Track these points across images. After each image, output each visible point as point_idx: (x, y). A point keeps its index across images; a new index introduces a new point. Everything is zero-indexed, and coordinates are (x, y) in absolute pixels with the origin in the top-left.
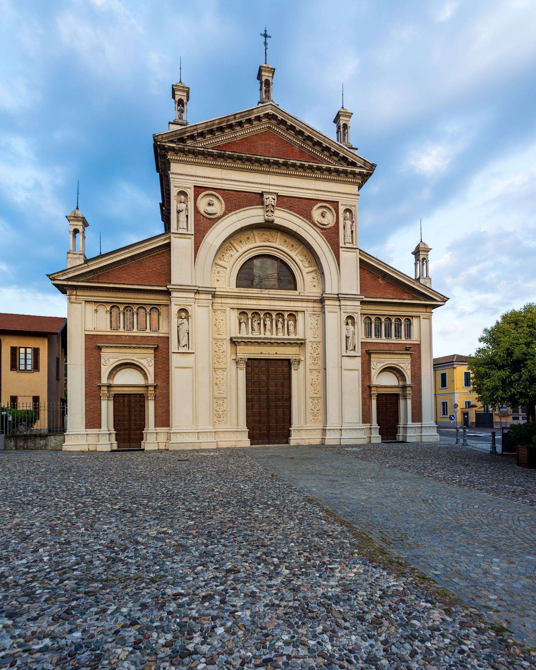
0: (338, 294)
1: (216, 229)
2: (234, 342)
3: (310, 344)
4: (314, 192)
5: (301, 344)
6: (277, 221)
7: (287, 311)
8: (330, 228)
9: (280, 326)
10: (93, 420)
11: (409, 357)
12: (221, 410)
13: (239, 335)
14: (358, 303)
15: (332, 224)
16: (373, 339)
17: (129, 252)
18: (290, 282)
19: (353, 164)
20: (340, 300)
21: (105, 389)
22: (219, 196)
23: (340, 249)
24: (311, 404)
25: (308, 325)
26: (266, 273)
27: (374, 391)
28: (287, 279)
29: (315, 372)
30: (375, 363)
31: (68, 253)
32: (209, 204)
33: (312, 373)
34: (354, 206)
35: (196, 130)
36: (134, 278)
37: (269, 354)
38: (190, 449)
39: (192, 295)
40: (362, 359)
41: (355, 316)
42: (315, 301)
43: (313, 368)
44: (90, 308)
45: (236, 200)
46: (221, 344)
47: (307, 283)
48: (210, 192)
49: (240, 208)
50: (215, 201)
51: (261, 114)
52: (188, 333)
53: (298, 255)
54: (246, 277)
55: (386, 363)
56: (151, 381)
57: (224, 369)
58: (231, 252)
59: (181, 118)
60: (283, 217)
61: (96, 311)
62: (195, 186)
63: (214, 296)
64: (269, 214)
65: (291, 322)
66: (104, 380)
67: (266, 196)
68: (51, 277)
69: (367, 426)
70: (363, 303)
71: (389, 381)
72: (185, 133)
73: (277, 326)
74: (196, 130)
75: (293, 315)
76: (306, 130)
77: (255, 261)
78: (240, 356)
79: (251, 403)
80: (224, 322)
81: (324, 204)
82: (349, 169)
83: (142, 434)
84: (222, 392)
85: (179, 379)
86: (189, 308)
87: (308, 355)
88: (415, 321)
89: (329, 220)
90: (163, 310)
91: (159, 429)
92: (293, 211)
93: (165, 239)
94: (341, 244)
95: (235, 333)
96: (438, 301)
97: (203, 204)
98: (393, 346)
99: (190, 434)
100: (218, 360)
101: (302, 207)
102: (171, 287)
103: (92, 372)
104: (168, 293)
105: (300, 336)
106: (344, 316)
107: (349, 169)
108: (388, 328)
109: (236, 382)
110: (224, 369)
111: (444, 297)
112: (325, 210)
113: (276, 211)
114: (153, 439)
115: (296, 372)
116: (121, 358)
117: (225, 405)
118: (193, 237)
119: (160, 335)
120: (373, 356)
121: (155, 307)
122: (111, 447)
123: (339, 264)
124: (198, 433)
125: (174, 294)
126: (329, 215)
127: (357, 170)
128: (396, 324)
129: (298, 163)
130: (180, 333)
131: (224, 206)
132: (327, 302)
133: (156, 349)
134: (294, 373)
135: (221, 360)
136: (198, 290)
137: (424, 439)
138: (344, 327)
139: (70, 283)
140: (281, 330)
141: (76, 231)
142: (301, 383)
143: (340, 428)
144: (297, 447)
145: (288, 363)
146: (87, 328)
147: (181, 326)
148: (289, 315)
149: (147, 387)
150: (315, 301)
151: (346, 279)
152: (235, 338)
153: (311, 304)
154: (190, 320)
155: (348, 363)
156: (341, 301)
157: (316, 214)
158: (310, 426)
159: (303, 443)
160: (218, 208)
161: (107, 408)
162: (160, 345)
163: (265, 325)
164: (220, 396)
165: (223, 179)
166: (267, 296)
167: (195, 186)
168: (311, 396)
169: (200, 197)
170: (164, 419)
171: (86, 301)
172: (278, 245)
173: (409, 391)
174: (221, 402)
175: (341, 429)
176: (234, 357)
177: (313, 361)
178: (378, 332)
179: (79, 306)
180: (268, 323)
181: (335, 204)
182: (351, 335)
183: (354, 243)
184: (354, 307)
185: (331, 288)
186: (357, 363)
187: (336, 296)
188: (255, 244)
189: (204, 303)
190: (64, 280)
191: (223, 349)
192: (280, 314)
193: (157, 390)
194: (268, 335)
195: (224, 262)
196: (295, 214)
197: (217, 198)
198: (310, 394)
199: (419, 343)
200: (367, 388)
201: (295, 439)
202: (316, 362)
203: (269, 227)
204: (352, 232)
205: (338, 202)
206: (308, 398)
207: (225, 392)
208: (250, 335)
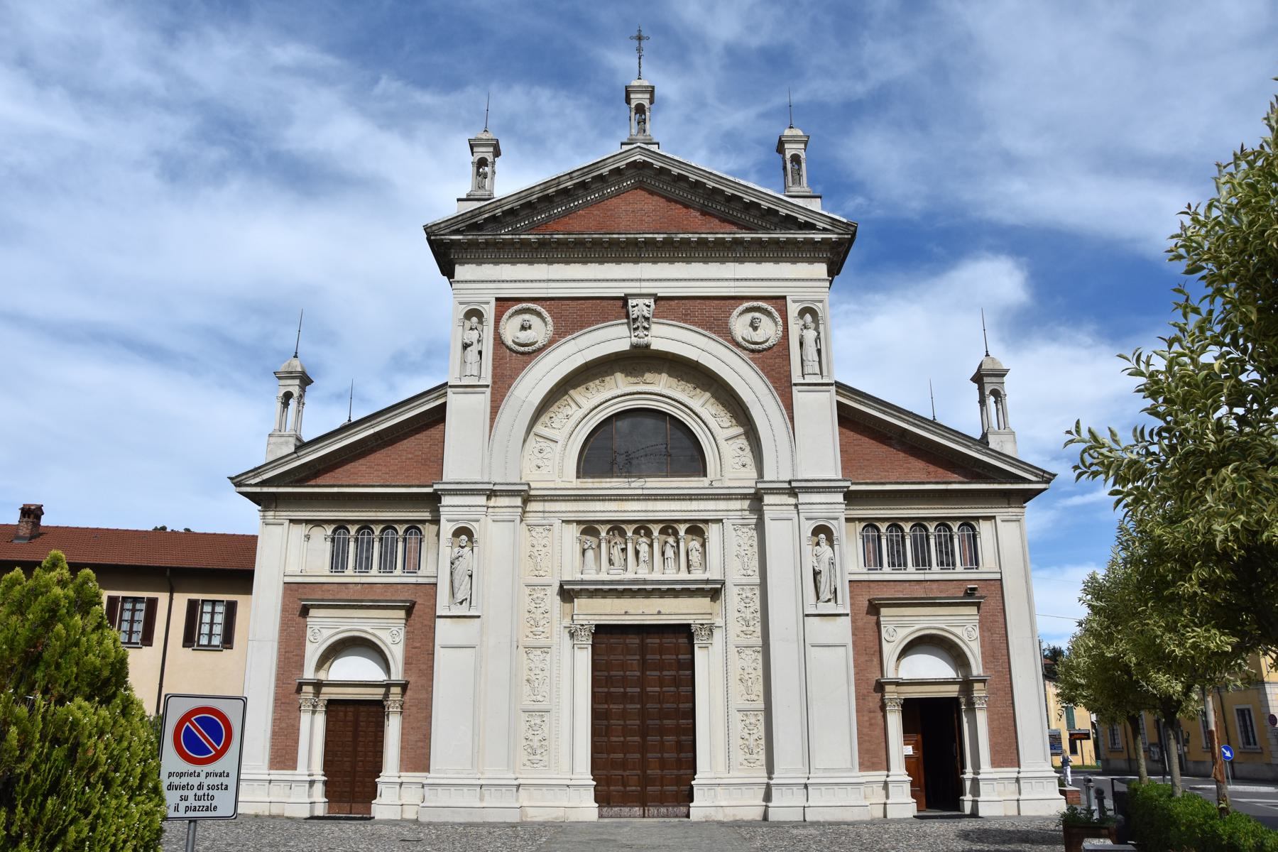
0: (790, 482)
1: (538, 367)
2: (567, 594)
3: (736, 590)
4: (732, 284)
5: (714, 592)
6: (657, 345)
7: (685, 521)
8: (770, 348)
9: (670, 552)
10: (283, 755)
11: (974, 610)
12: (537, 738)
13: (578, 577)
14: (839, 498)
16: (887, 573)
17: (372, 427)
19: (809, 226)
21: (310, 689)
22: (545, 314)
23: (794, 388)
24: (741, 725)
25: (732, 548)
26: (638, 445)
27: (891, 692)
28: (685, 453)
29: (749, 651)
30: (891, 628)
31: (270, 435)
32: (523, 328)
33: (743, 655)
34: (821, 301)
35: (500, 206)
36: (372, 478)
37: (643, 614)
38: (462, 820)
39: (482, 500)
40: (853, 622)
41: (832, 525)
42: (744, 497)
43: (745, 644)
44: (301, 530)
45: (573, 314)
46: (541, 595)
47: (727, 459)
48: (524, 305)
49: (582, 328)
50: (534, 320)
52: (471, 576)
53: (708, 405)
54: (604, 452)
55: (917, 627)
56: (397, 674)
57: (545, 649)
58: (568, 411)
59: (481, 187)
60: (667, 337)
61: (308, 537)
62: (498, 299)
63: (527, 499)
64: (641, 333)
66: (309, 673)
67: (631, 302)
68: (237, 481)
69: (880, 776)
70: (852, 498)
72: (480, 214)
73: (663, 554)
74: (500, 206)
75: (696, 529)
76: (709, 179)
77: (619, 424)
78: (580, 620)
79: (605, 722)
80: (549, 549)
81: (755, 304)
82: (800, 236)
83: (375, 786)
84: (539, 698)
85: (449, 668)
86: (474, 527)
87: (732, 615)
88: (984, 529)
89: (768, 331)
90: (428, 530)
91: (408, 777)
92: (691, 323)
93: (437, 398)
94: (796, 378)
95: (572, 571)
96: (1030, 482)
97: (511, 331)
98: (935, 585)
99: (465, 789)
100: (534, 629)
101: (709, 313)
102: (441, 487)
103: (290, 655)
104: (433, 500)
105: (714, 574)
106: (808, 527)
107: (800, 236)
108: (922, 546)
109: (573, 674)
110: (545, 649)
111: (1044, 472)
112: (757, 315)
113: (654, 327)
114: (395, 796)
115: (705, 651)
116: (343, 628)
117: (546, 727)
118: (489, 390)
119: (421, 580)
120: (884, 611)
121: (413, 526)
122: (312, 810)
123: (792, 419)
124: (481, 786)
125: (446, 500)
127: (818, 237)
128: (915, 537)
130: (456, 577)
131: (550, 327)
132: (768, 499)
133: (409, 610)
134: (699, 655)
135: (541, 629)
136: (492, 490)
137: (1027, 810)
138: (808, 549)
139: (265, 490)
140: (671, 563)
141: (288, 396)
142: (717, 680)
143: (805, 781)
144: (707, 824)
145: (685, 632)
146: (289, 570)
147: (457, 563)
148: (688, 531)
149: (388, 686)
150: (744, 497)
151: (810, 445)
152: (569, 582)
153: (737, 505)
154: (836, 547)
156: (800, 496)
157: (740, 326)
158: (738, 775)
159: (720, 816)
160: (539, 332)
161: (313, 730)
162: (419, 601)
163: (637, 553)
164: (536, 708)
165: (549, 281)
166: (640, 492)
167: (498, 299)
168: (741, 707)
170: (418, 757)
171: (291, 521)
172: (660, 389)
173: (979, 691)
174: (538, 721)
175: (806, 786)
176: (567, 622)
177: (745, 628)
178: (947, 554)
179: (278, 529)
180: (644, 549)
181: (780, 301)
183: (825, 373)
184: (832, 507)
185: (776, 471)
186: (842, 630)
187: (786, 485)
188: (615, 393)
191: (544, 607)
192: (669, 527)
193: (409, 693)
194: (643, 573)
195: (553, 431)
196: (700, 330)
197: (539, 314)
198: (738, 701)
199: (998, 576)
200: (873, 689)
201: (703, 805)
202: (752, 628)
203: (640, 360)
204: (819, 351)
205: (784, 298)
206: (733, 712)
207: (547, 699)
208: (603, 576)
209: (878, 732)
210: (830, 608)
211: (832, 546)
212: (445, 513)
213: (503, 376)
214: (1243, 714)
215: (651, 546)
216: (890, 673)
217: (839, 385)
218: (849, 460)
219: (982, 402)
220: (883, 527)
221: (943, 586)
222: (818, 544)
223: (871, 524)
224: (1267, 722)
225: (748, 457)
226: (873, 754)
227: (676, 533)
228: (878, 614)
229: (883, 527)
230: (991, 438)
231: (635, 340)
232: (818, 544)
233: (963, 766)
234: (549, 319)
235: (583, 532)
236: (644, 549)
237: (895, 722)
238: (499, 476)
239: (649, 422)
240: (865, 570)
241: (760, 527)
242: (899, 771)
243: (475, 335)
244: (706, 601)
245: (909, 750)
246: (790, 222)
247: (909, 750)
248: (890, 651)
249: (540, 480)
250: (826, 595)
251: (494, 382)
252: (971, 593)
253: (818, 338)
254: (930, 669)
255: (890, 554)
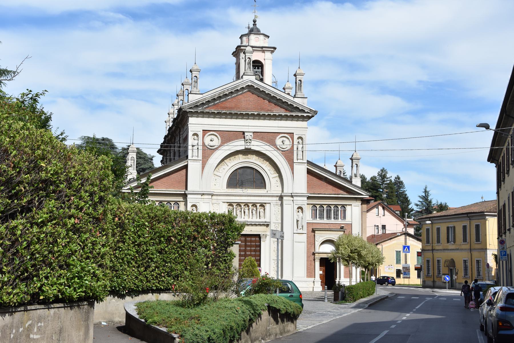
3: (274, 224)
4: (277, 128)
6: (253, 148)
9: (254, 212)
15: (289, 147)
16: (318, 221)
18: (262, 183)
19: (303, 111)
20: (293, 197)
28: (257, 180)
30: (318, 237)
32: (211, 140)
39: (200, 196)
41: (303, 207)
42: (277, 196)
51: (244, 86)
58: (224, 167)
60: (256, 145)
64: (248, 144)
65: (262, 210)
67: (246, 134)
69: (312, 279)
71: (329, 249)
88: (348, 208)
89: (287, 145)
94: (295, 161)
96: (363, 195)
97: (207, 141)
98: (332, 225)
101: (269, 138)
123: (293, 173)
126: (287, 142)
129: (267, 114)
131: (220, 141)
132: (285, 198)
134: (262, 243)
140: (255, 215)
148: (260, 206)
150: (277, 196)
151: (298, 181)
155: (297, 237)
157: (278, 141)
160: (216, 142)
163: (244, 212)
169: (206, 136)
172: (253, 161)
180: (247, 211)
182: (300, 219)
184: (303, 201)
185: (287, 190)
189: (207, 201)
190: (127, 189)
192: (254, 205)
197: (216, 136)
203: (247, 152)
209: (313, 267)
210: (301, 231)
211: (302, 212)
212: (189, 200)
213: (205, 156)
214: (478, 262)
215: (249, 210)
216: (317, 250)
217: (309, 163)
218: (309, 185)
219: (352, 167)
220: (318, 206)
221: (334, 225)
222: (298, 212)
223: (314, 205)
224: (486, 267)
225: (278, 179)
226: (311, 273)
227: (256, 206)
228: (315, 232)
229: (318, 206)
230: (353, 180)
231: (246, 147)
232: (298, 212)
233: (336, 278)
234: (220, 138)
235: (229, 205)
236: (247, 211)
237: (317, 264)
238: (204, 190)
239: (249, 170)
240: (312, 219)
241: (282, 205)
242: (318, 279)
243: (196, 142)
244: (265, 227)
245: (321, 272)
246: (297, 109)
247: (321, 272)
248: (317, 244)
249: (216, 191)
250: (300, 227)
251: (203, 159)
252: (342, 228)
253: (303, 147)
254: (329, 249)
255: (320, 215)
